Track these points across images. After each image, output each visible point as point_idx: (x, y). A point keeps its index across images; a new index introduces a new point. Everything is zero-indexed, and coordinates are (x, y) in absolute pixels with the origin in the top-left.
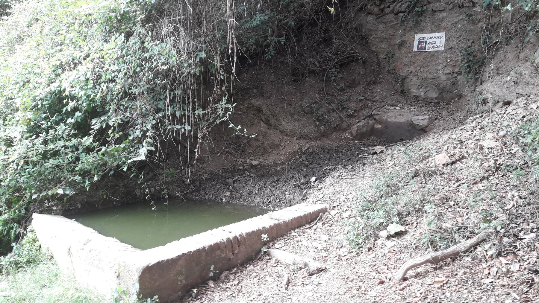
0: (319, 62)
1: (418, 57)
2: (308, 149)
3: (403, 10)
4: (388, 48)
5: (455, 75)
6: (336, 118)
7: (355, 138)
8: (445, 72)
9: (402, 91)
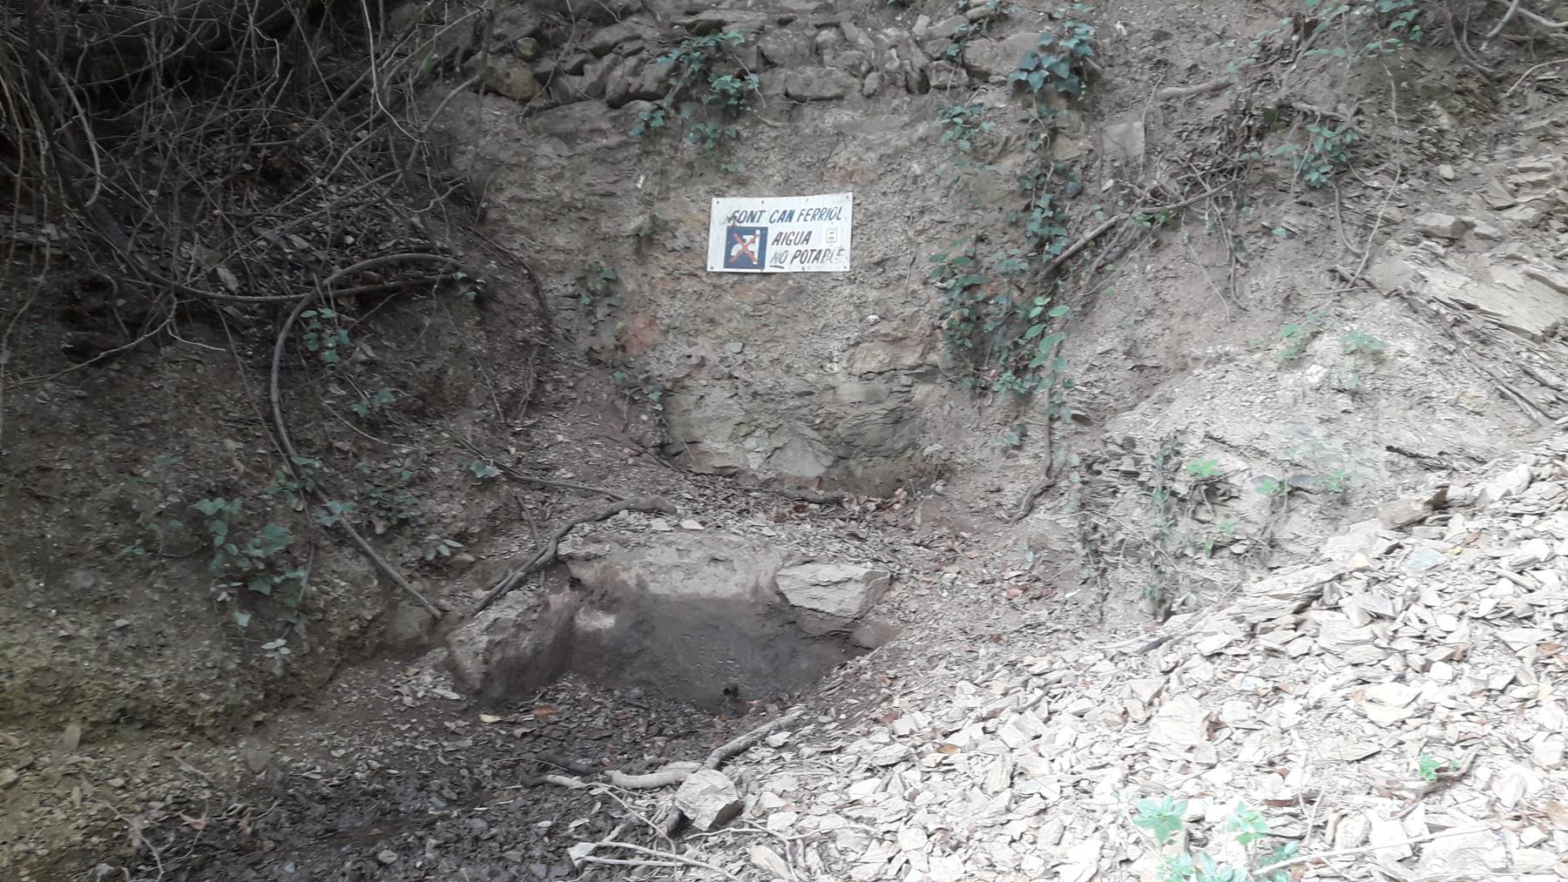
0: (237, 268)
1: (728, 299)
2: (172, 821)
3: (650, 85)
4: (586, 250)
5: (904, 380)
6: (357, 585)
7: (478, 697)
8: (859, 367)
9: (662, 446)
